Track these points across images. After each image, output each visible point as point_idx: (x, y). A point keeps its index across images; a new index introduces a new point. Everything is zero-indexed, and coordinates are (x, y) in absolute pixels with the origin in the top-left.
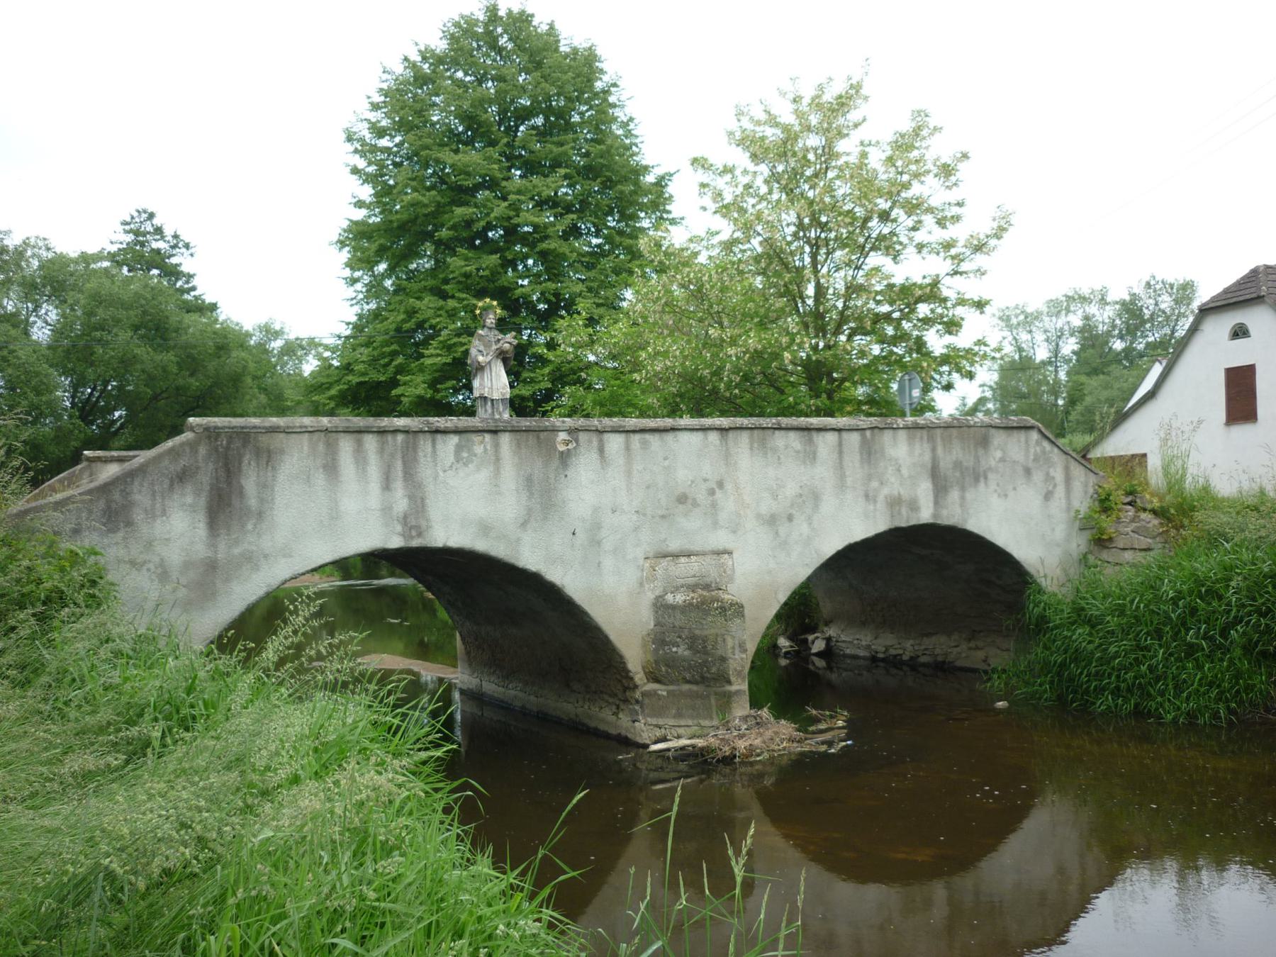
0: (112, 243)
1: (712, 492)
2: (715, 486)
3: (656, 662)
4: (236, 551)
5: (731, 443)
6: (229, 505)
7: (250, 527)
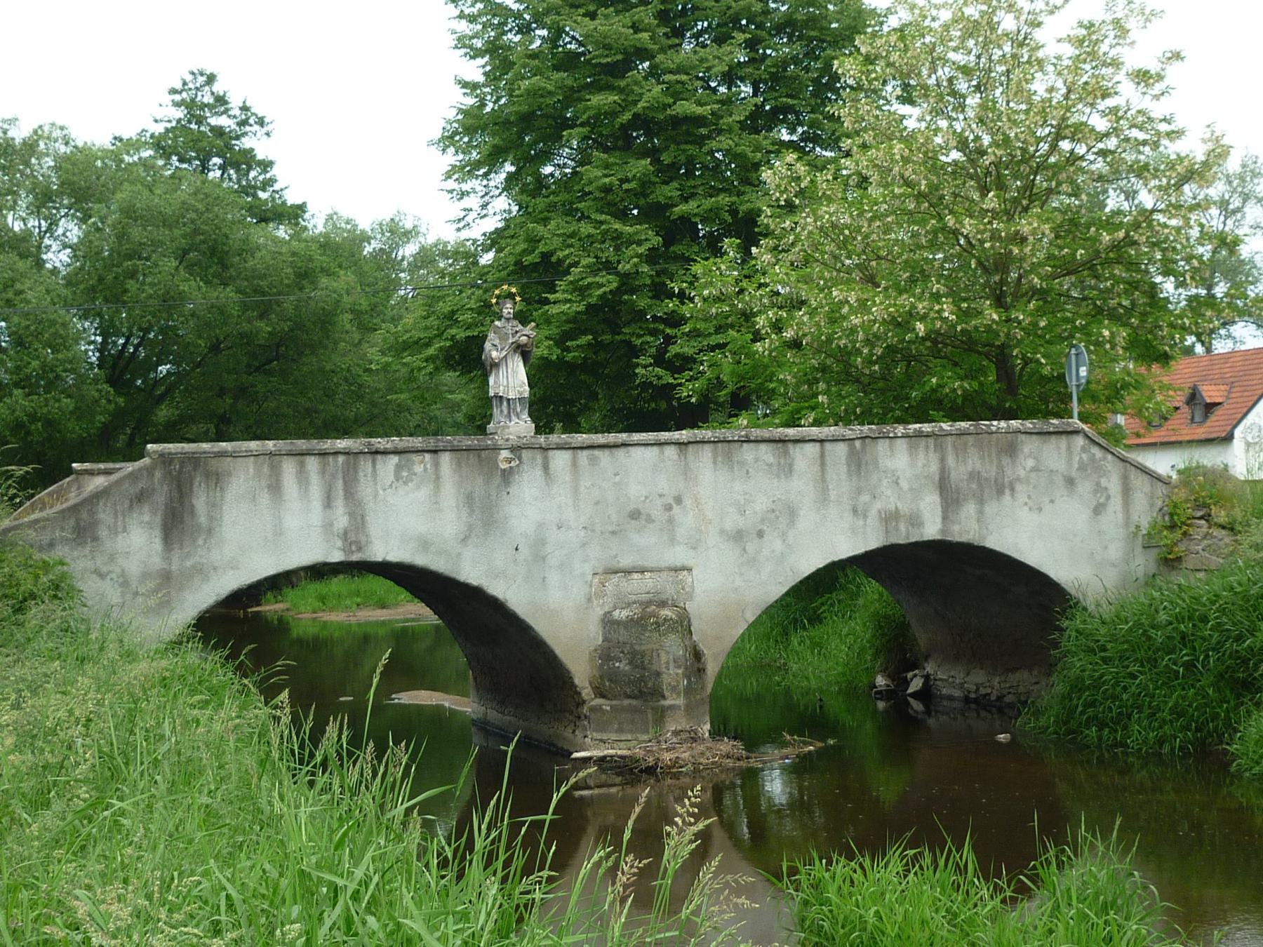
0: (156, 121)
1: (669, 508)
2: (672, 502)
3: (601, 677)
4: (188, 563)
5: (690, 457)
6: (182, 522)
7: (200, 542)
